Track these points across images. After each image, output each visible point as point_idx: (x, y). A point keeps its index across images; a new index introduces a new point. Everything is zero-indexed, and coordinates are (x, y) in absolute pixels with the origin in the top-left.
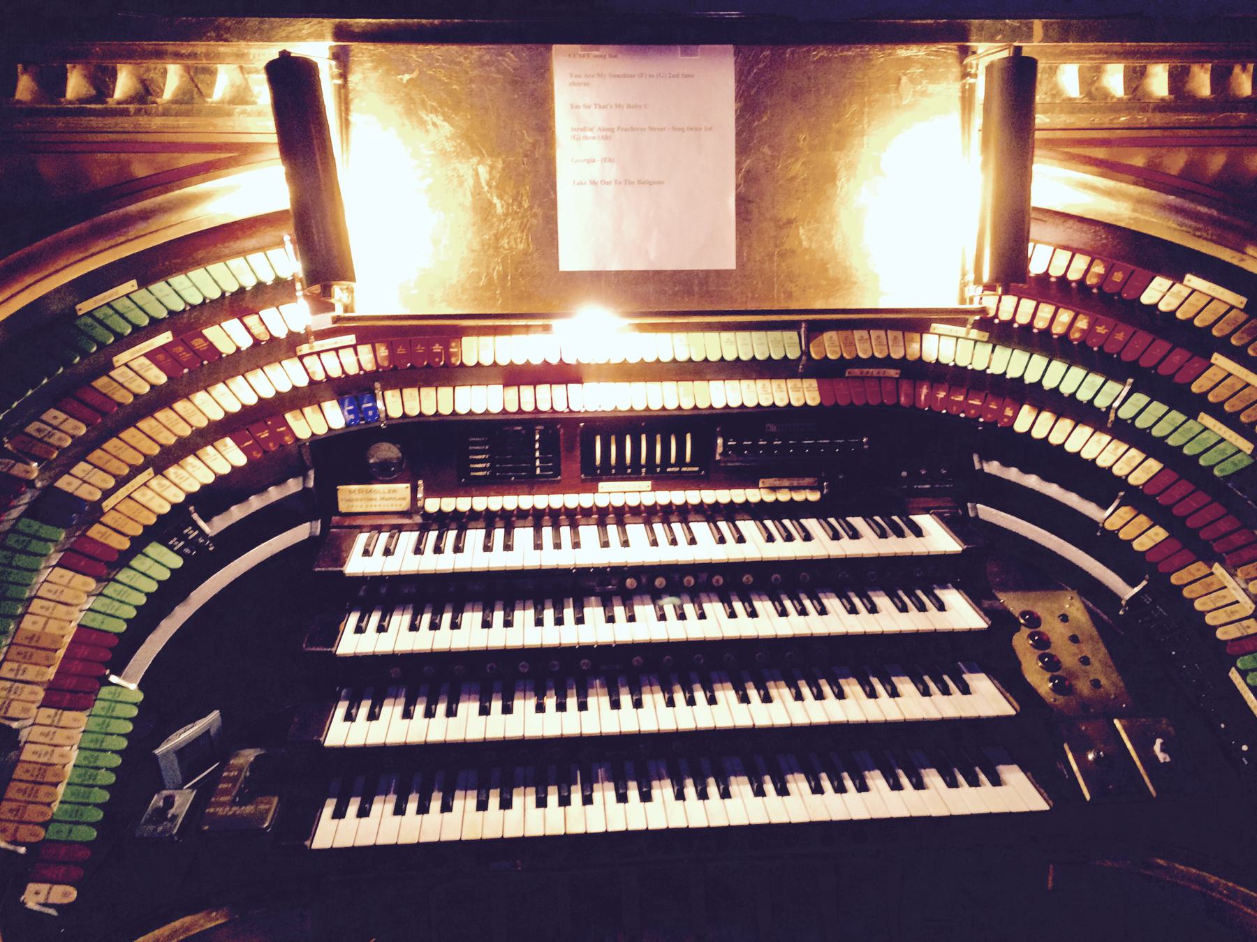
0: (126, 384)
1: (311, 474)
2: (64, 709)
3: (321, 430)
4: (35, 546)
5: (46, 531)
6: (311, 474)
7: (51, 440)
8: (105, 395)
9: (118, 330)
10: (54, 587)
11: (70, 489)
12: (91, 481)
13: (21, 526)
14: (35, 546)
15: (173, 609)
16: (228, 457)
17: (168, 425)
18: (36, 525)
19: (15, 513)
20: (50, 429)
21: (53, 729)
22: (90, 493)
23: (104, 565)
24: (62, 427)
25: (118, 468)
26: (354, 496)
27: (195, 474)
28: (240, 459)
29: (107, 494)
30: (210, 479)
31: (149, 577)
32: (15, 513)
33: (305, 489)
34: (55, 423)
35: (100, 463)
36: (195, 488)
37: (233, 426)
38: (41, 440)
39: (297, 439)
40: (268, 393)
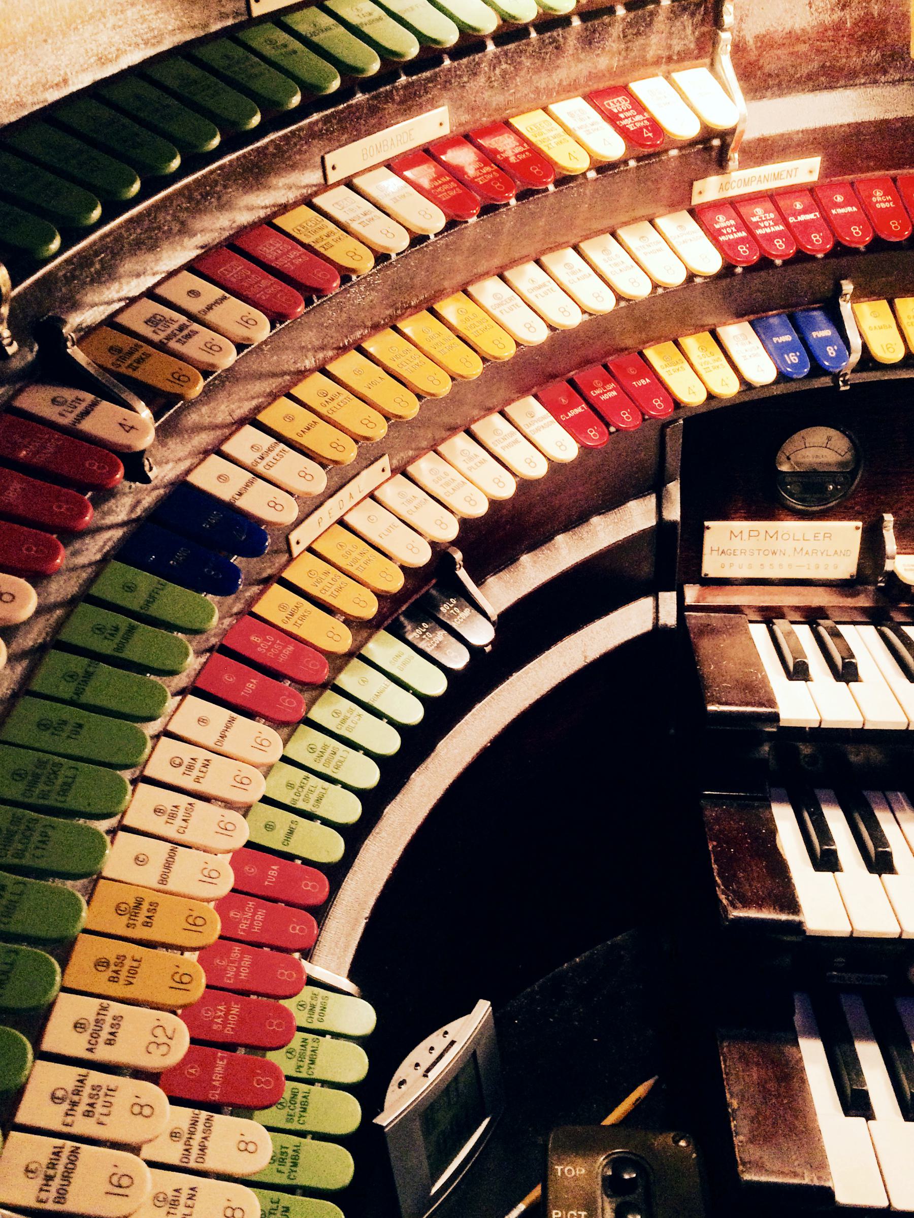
0: (355, 226)
1: (674, 488)
2: (215, 1108)
3: (727, 388)
4: (143, 644)
5: (176, 600)
6: (674, 488)
7: (192, 349)
8: (308, 247)
9: (350, 60)
10: (185, 751)
11: (225, 493)
12: (271, 473)
13: (105, 589)
14: (143, 644)
15: (408, 778)
16: (537, 442)
17: (427, 353)
18: (145, 581)
19: (92, 549)
20: (183, 319)
21: (67, 712)
22: (273, 505)
23: (274, 683)
24: (211, 317)
25: (334, 446)
26: (737, 544)
27: (472, 479)
28: (565, 448)
29: (310, 507)
30: (506, 489)
31: (379, 714)
32: (92, 549)
33: (662, 525)
34: (194, 306)
35: (289, 432)
36: (480, 509)
37: (561, 370)
38: (161, 347)
39: (678, 405)
40: (638, 288)
